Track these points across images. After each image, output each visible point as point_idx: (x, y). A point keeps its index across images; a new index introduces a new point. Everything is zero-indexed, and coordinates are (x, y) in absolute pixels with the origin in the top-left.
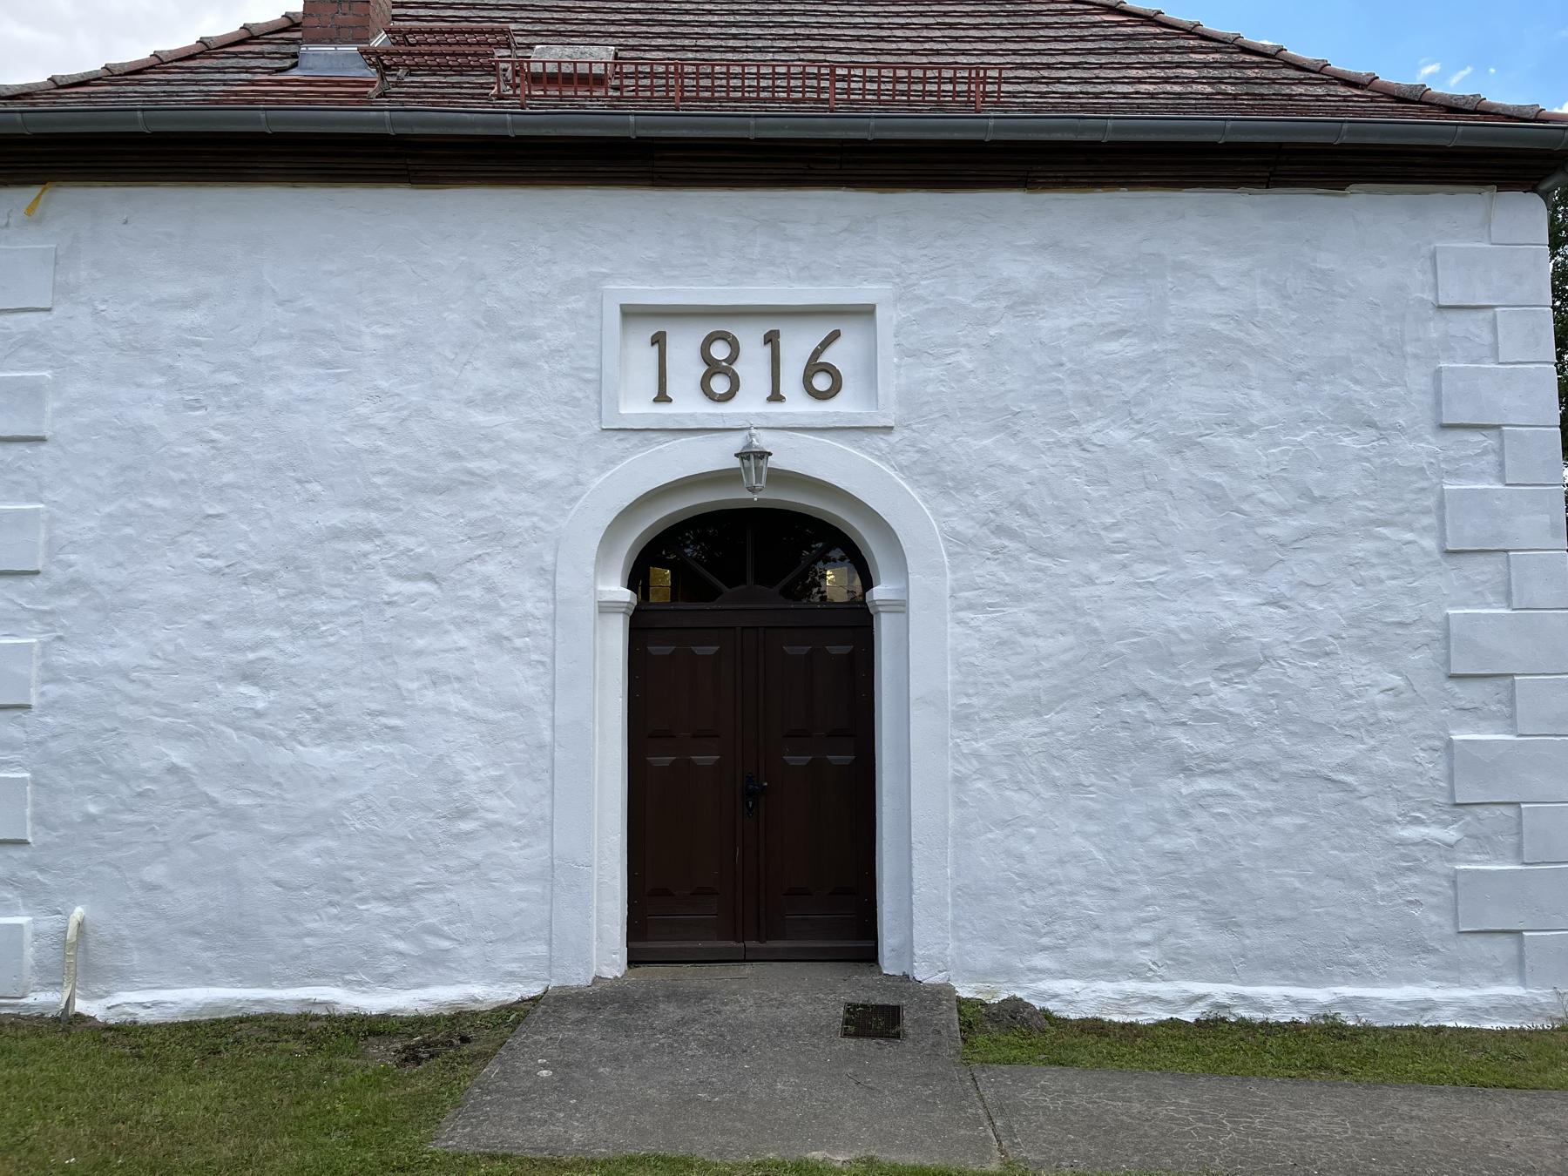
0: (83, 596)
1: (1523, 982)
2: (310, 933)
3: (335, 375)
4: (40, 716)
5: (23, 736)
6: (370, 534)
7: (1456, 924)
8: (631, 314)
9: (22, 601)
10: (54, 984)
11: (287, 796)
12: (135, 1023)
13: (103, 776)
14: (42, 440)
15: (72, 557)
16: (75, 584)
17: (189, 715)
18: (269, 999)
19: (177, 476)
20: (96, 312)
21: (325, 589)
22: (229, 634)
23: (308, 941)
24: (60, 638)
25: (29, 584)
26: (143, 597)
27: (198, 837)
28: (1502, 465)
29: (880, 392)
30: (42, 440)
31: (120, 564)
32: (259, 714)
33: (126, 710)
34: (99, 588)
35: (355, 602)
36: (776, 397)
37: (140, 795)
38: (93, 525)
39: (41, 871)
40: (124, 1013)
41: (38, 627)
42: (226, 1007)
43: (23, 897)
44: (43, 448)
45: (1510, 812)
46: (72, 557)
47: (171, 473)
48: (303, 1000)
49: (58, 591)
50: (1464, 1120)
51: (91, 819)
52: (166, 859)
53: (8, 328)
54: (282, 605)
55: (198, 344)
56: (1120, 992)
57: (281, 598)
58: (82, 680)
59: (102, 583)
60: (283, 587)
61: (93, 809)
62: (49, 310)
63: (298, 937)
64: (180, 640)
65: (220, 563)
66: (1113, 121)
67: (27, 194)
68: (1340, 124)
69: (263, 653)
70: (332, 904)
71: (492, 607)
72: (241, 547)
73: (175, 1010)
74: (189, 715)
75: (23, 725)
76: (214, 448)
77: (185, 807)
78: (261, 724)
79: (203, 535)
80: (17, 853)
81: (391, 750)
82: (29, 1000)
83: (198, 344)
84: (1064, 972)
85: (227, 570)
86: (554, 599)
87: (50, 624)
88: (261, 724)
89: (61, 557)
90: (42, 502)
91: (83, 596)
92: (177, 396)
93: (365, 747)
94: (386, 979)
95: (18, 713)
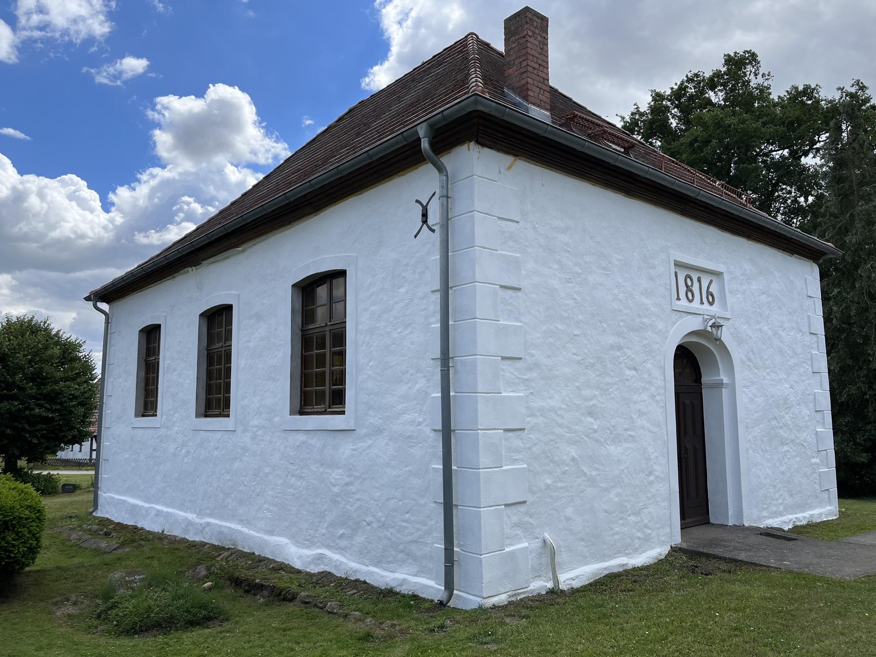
0: (539, 371)
1: (830, 506)
2: (617, 533)
3: (607, 274)
4: (528, 434)
5: (522, 445)
6: (620, 348)
7: (821, 489)
8: (678, 264)
9: (516, 373)
10: (537, 576)
11: (606, 470)
12: (572, 588)
13: (551, 464)
14: (519, 289)
15: (534, 352)
16: (537, 365)
17: (575, 432)
18: (609, 566)
19: (566, 315)
20: (534, 228)
21: (609, 372)
22: (584, 393)
23: (616, 537)
24: (532, 393)
25: (518, 364)
26: (558, 373)
27: (582, 492)
28: (818, 346)
29: (728, 305)
30: (519, 289)
31: (549, 357)
32: (595, 431)
33: (558, 430)
34: (544, 368)
35: (617, 379)
36: (702, 303)
37: (564, 473)
38: (539, 336)
39: (531, 517)
40: (567, 585)
41: (523, 388)
42: (597, 574)
43: (524, 532)
44: (519, 294)
45: (825, 452)
46: (534, 352)
47: (563, 313)
48: (619, 565)
49: (529, 369)
50: (313, 613)
51: (548, 487)
52: (572, 504)
53: (503, 228)
54: (598, 379)
55: (568, 252)
56: (780, 521)
57: (597, 376)
58: (541, 415)
59: (544, 365)
60: (597, 370)
61: (549, 482)
62: (518, 222)
63: (613, 535)
64: (570, 395)
65: (579, 358)
66: (552, 128)
67: (508, 159)
68: (547, 126)
69: (594, 402)
70: (621, 519)
71: (650, 383)
72: (586, 351)
73: (584, 579)
74: (575, 432)
75: (522, 439)
76: (576, 302)
77: (576, 477)
78: (596, 435)
79: (573, 344)
80: (522, 508)
81: (632, 446)
82: (531, 587)
83: (568, 252)
84: (769, 517)
85: (581, 362)
86: (665, 379)
87: (527, 386)
88: (596, 435)
89: (529, 351)
90: (521, 322)
91: (539, 371)
92: (563, 276)
93: (626, 445)
94: (636, 550)
95: (519, 433)
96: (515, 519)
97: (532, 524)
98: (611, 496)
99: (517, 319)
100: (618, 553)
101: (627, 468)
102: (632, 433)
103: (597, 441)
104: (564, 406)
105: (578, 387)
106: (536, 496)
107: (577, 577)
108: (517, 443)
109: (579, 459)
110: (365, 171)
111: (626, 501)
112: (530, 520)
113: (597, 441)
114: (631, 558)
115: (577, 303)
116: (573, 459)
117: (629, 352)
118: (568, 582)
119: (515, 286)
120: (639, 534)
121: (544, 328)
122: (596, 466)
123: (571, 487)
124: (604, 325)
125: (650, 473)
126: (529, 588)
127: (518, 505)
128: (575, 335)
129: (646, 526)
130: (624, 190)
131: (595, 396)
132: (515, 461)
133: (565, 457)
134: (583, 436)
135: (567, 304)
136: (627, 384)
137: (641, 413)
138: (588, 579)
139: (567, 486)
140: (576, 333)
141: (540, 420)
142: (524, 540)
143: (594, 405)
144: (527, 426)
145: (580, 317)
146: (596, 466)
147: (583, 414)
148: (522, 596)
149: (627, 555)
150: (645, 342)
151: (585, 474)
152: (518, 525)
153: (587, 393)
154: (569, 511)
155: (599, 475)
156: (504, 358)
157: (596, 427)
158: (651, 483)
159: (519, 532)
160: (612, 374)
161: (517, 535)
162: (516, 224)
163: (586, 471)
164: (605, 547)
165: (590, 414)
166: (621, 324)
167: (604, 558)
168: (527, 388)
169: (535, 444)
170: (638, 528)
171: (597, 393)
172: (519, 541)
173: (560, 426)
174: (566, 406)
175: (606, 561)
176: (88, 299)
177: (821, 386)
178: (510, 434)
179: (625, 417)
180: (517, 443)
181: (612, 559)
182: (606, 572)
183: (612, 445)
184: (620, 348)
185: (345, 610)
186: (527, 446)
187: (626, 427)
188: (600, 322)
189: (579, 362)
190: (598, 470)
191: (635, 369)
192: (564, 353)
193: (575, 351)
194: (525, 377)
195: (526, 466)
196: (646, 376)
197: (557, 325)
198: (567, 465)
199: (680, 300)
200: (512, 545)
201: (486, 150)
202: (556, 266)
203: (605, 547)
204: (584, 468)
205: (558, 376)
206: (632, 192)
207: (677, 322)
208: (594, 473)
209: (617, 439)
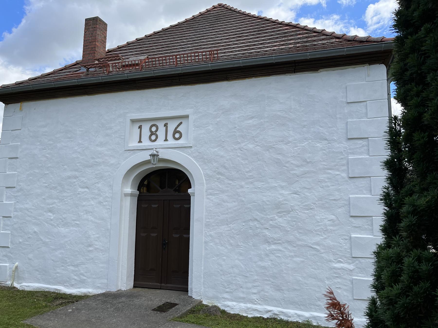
2: (58, 273)
6: (76, 177)
8: (133, 121)
14: (17, 158)
15: (21, 184)
16: (21, 190)
17: (39, 220)
23: (57, 274)
26: (32, 192)
27: (39, 248)
30: (17, 158)
32: (52, 220)
33: (28, 218)
35: (72, 194)
37: (29, 238)
44: (18, 160)
46: (21, 184)
48: (55, 289)
49: (18, 191)
51: (20, 243)
55: (46, 135)
57: (58, 193)
58: (21, 211)
60: (58, 190)
61: (21, 240)
63: (56, 273)
65: (47, 185)
67: (18, 105)
69: (53, 206)
70: (62, 266)
72: (51, 181)
78: (52, 222)
79: (44, 178)
80: (7, 249)
83: (46, 135)
85: (48, 186)
87: (16, 199)
88: (52, 222)
90: (17, 172)
94: (72, 286)
96: (4, 253)
97: (12, 257)
98: (57, 253)
99: (15, 171)
100: (59, 283)
101: (70, 240)
102: (78, 222)
103: (52, 225)
104: (33, 208)
105: (44, 199)
106: (14, 246)
107: (29, 286)
108: (9, 223)
109: (39, 233)
110: (212, 79)
111: (66, 258)
112: (11, 255)
113: (52, 225)
114: (68, 288)
115: (48, 159)
116: (35, 232)
117: (83, 179)
118: (24, 287)
119: (14, 157)
120: (76, 278)
121: (28, 173)
122: (49, 237)
123: (32, 245)
124: (66, 167)
125: (90, 246)
126: (6, 283)
127: (6, 248)
128: (46, 174)
129: (82, 274)
130: (78, 94)
131: (55, 203)
132: (6, 230)
133: (30, 231)
134: (43, 222)
135: (42, 160)
136: (79, 196)
137: (87, 212)
138: (34, 289)
139: (30, 244)
140: (46, 173)
141: (19, 213)
142: (8, 263)
143: (53, 207)
144: (12, 216)
145: (49, 165)
146: (49, 237)
147: (45, 211)
148: (3, 285)
149: (65, 286)
150: (97, 172)
151: (42, 240)
152: (5, 256)
153: (50, 201)
154: (31, 256)
155: (51, 241)
156: (7, 188)
157: (52, 218)
158: (90, 251)
159: (6, 259)
160: (69, 191)
161: (5, 260)
162: (19, 130)
163: (42, 238)
164: (50, 278)
165: (50, 211)
166: (78, 164)
167: (49, 283)
168: (16, 199)
169: (15, 224)
170: (75, 274)
171: (56, 201)
172: (6, 262)
173: (29, 216)
174: (34, 207)
175: (51, 285)
176: (150, 155)
177: (371, 191)
178: (5, 218)
179: (74, 213)
180: (9, 223)
181: (54, 285)
182: (47, 290)
183: (62, 228)
184: (76, 177)
185: (336, 312)
186: (12, 224)
187: (74, 219)
188: (63, 165)
189: (46, 187)
190: (50, 239)
191: (87, 188)
192: (38, 183)
193: (44, 181)
194: (16, 195)
195: (10, 232)
196: (96, 191)
197: (35, 171)
198: (31, 234)
199: (142, 142)
200: (2, 263)
201: (9, 105)
202: (39, 144)
203: (50, 278)
204: (42, 238)
205: (32, 194)
206: (89, 92)
207: (129, 157)
208: (47, 240)
209: (66, 224)
